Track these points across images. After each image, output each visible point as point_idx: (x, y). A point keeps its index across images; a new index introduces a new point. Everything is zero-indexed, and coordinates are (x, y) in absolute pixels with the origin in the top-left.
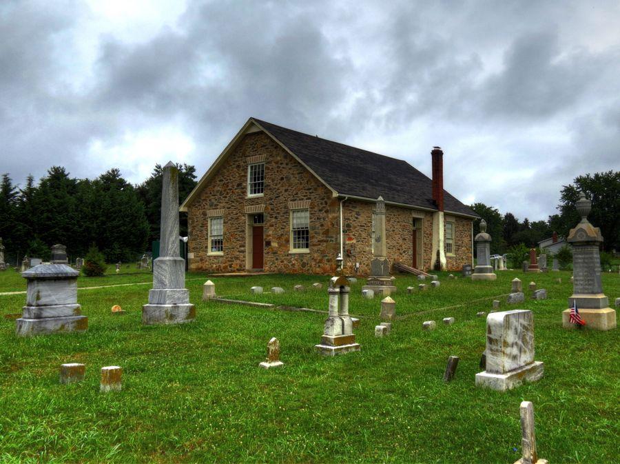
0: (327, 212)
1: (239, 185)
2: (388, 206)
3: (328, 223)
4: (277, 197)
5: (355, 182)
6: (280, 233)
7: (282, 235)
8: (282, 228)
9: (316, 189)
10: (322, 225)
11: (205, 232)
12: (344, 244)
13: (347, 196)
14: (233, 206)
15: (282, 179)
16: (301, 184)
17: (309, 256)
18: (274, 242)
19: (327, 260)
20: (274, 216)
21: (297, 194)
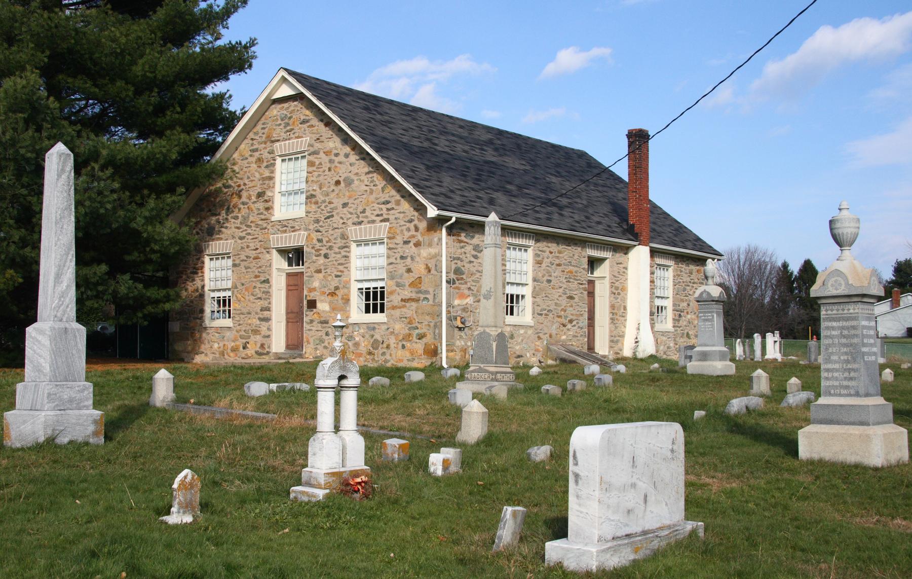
0: (417, 244)
1: (260, 195)
2: (506, 230)
3: (419, 269)
4: (328, 218)
5: (473, 189)
6: (334, 282)
7: (337, 288)
8: (337, 276)
10: (409, 271)
12: (449, 305)
13: (454, 216)
14: (249, 234)
15: (338, 183)
16: (372, 192)
17: (384, 327)
18: (322, 301)
19: (418, 335)
20: (323, 252)
21: (364, 212)
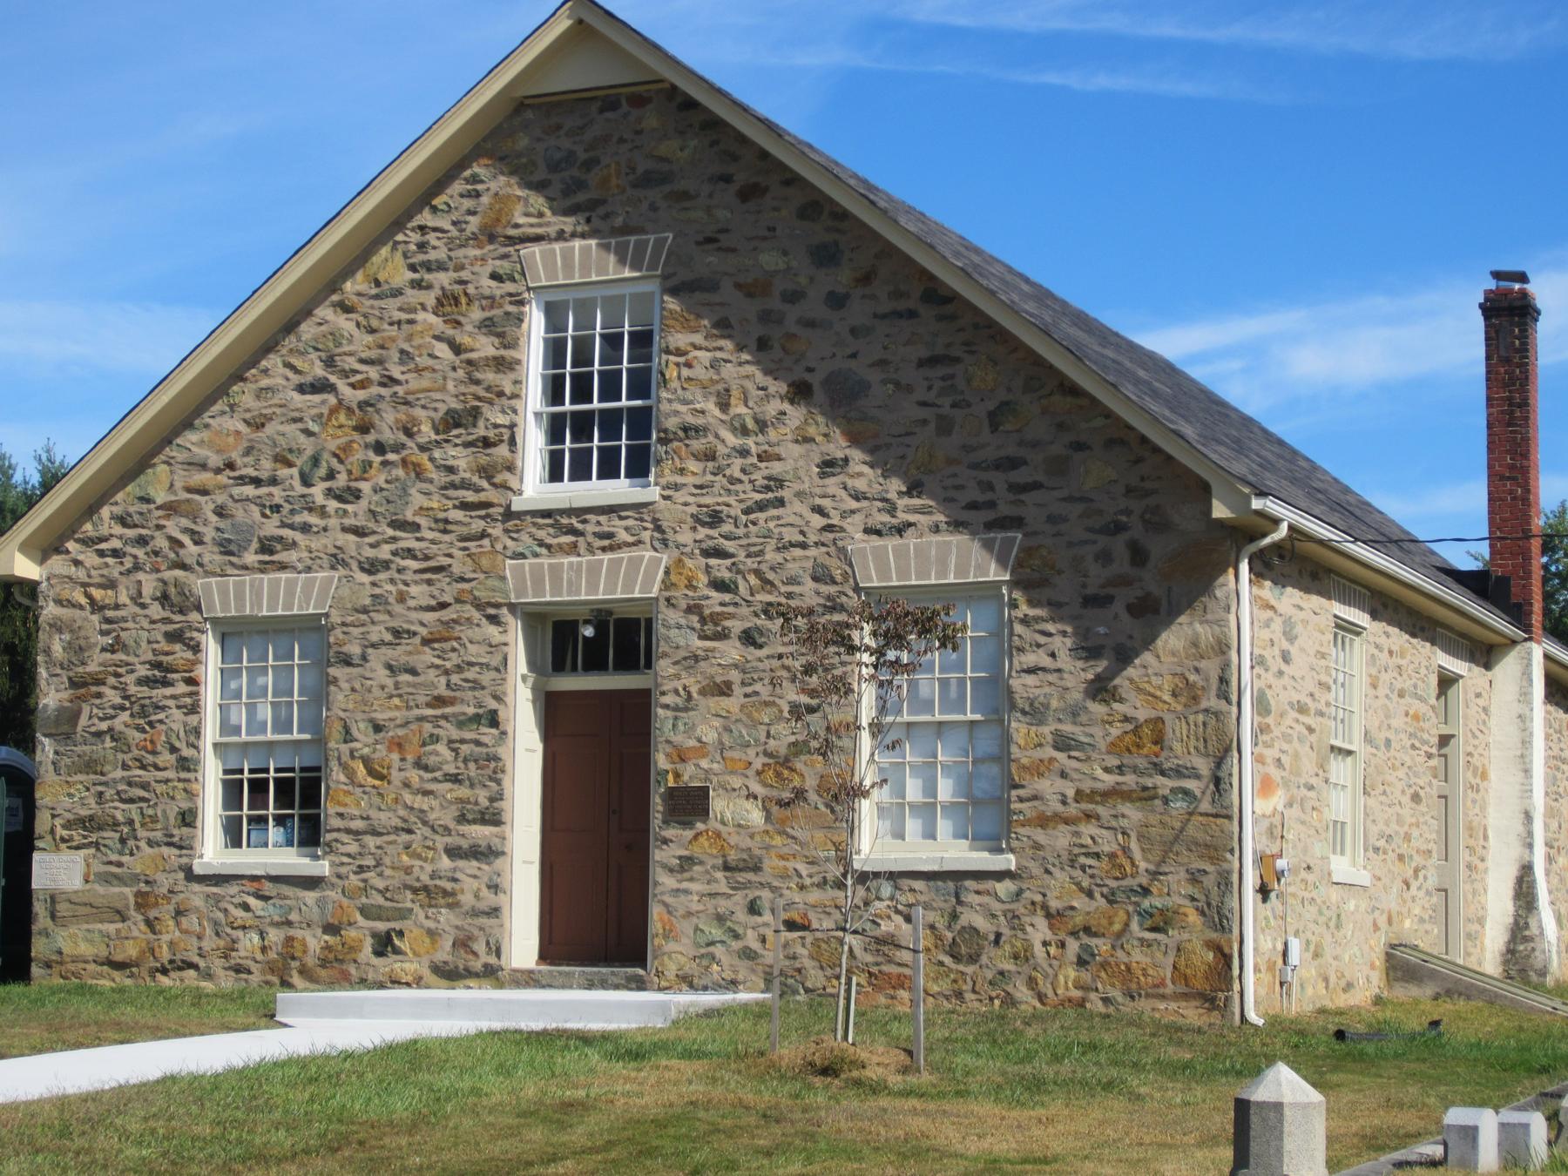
4: (761, 507)
9: (1059, 467)
11: (176, 718)
14: (410, 553)
20: (736, 626)
